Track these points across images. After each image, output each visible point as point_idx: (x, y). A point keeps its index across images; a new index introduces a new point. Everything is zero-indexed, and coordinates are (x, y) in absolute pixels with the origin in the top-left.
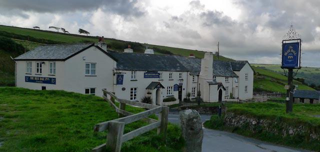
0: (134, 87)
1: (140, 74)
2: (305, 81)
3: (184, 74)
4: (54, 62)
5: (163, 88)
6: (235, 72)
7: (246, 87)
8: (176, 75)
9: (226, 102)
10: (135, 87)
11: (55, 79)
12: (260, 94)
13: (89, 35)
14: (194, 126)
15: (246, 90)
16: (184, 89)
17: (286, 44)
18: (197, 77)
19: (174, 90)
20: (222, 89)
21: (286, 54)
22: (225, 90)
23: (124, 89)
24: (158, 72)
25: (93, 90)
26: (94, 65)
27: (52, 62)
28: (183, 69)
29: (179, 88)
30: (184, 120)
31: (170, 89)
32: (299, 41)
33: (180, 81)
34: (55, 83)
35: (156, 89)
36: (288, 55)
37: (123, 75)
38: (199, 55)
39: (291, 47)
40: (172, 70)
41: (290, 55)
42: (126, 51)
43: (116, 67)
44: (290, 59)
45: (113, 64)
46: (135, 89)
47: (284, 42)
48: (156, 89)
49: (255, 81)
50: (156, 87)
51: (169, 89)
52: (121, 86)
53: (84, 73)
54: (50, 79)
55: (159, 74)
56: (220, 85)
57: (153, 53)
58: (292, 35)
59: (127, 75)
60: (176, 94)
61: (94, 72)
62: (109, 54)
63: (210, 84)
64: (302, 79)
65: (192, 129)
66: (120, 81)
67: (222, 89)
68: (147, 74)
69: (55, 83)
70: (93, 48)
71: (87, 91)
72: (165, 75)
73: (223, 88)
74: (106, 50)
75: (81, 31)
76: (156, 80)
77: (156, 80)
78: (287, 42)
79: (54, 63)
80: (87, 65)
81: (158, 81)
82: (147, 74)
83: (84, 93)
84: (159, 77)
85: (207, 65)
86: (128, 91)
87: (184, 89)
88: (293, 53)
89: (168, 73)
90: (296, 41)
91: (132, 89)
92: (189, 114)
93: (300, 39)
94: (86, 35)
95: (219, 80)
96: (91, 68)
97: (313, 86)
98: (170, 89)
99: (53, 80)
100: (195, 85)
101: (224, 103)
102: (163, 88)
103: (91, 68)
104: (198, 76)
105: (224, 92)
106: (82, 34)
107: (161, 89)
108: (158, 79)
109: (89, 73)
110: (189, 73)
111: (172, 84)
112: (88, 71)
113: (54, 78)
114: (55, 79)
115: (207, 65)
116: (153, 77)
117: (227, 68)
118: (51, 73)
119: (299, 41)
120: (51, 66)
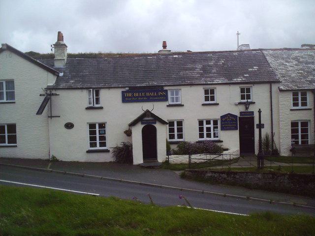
51: (205, 126)
82: (130, 95)
110: (275, 87)
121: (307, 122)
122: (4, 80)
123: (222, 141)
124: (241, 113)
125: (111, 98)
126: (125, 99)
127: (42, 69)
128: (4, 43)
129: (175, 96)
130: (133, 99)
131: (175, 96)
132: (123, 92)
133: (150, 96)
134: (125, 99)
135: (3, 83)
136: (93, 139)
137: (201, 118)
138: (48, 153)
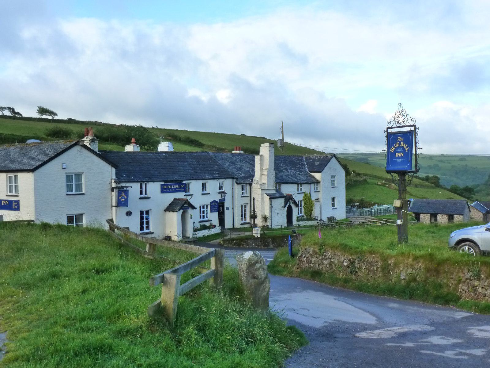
0: (144, 209)
1: (154, 188)
2: (442, 182)
3: (227, 184)
4: (16, 174)
5: (194, 208)
6: (311, 173)
7: (333, 199)
8: (212, 185)
9: (299, 226)
10: (147, 209)
11: (18, 202)
12: (264, 296)
13: (56, 118)
14: (257, 273)
15: (333, 205)
16: (228, 209)
17: (392, 133)
18: (248, 187)
19: (211, 211)
20: (293, 206)
21: (392, 149)
22: (297, 205)
23: (129, 214)
24: (184, 182)
25: (79, 217)
26: (79, 176)
27: (13, 175)
28: (224, 175)
29: (219, 207)
30: (243, 266)
31: (205, 210)
32: (413, 128)
33: (220, 195)
34: (18, 209)
35: (181, 211)
36: (395, 151)
37: (128, 191)
38: (250, 147)
39: (400, 139)
40: (207, 176)
41: (399, 152)
42: (129, 148)
43: (114, 177)
44: (399, 158)
45: (110, 172)
46: (147, 212)
47: (390, 131)
48: (181, 211)
49: (349, 186)
50: (181, 208)
51: (202, 210)
52: (124, 210)
53: (64, 191)
54: (10, 202)
55: (185, 184)
56: (288, 199)
57: (172, 150)
58: (401, 119)
59: (134, 188)
60: (214, 217)
61: (79, 187)
62: (104, 156)
63: (271, 199)
64: (436, 177)
65: (254, 278)
66: (122, 202)
67: (293, 206)
68: (165, 187)
69: (18, 209)
70: (77, 148)
71: (70, 219)
72: (195, 186)
73: (294, 202)
74: (97, 150)
75: (42, 111)
76: (180, 195)
77: (180, 195)
78: (394, 130)
79: (16, 177)
80: (69, 177)
81: (185, 198)
82: (165, 187)
83: (64, 222)
84: (185, 191)
85: (263, 164)
86: (136, 217)
87: (228, 209)
88: (403, 148)
89: (200, 182)
90: (408, 129)
91: (142, 213)
92: (249, 259)
93: (415, 126)
94: (50, 117)
95: (287, 189)
96: (73, 183)
97: (454, 190)
98: (205, 210)
99: (14, 204)
100: (246, 201)
101: (296, 230)
102: (194, 208)
103: (73, 183)
104: (250, 184)
105: (295, 210)
106: (44, 117)
107: (190, 211)
108: (184, 193)
109: (72, 191)
110: (235, 180)
111: (207, 200)
112: (69, 188)
113: (16, 201)
114: (18, 202)
115: (263, 164)
116: (175, 191)
117: (299, 168)
118: (11, 191)
119: (413, 128)
120: (10, 181)
121: (149, 211)
122: (74, 214)
123: (211, 221)
124: (220, 199)
125: (154, 188)
126: (163, 191)
127: (96, 156)
128: (39, 106)
129: (204, 187)
130: (167, 190)
131: (204, 187)
132: (162, 185)
133: (176, 188)
134: (163, 191)
135: (73, 216)
136: (142, 223)
137: (142, 209)
138: (300, 313)
